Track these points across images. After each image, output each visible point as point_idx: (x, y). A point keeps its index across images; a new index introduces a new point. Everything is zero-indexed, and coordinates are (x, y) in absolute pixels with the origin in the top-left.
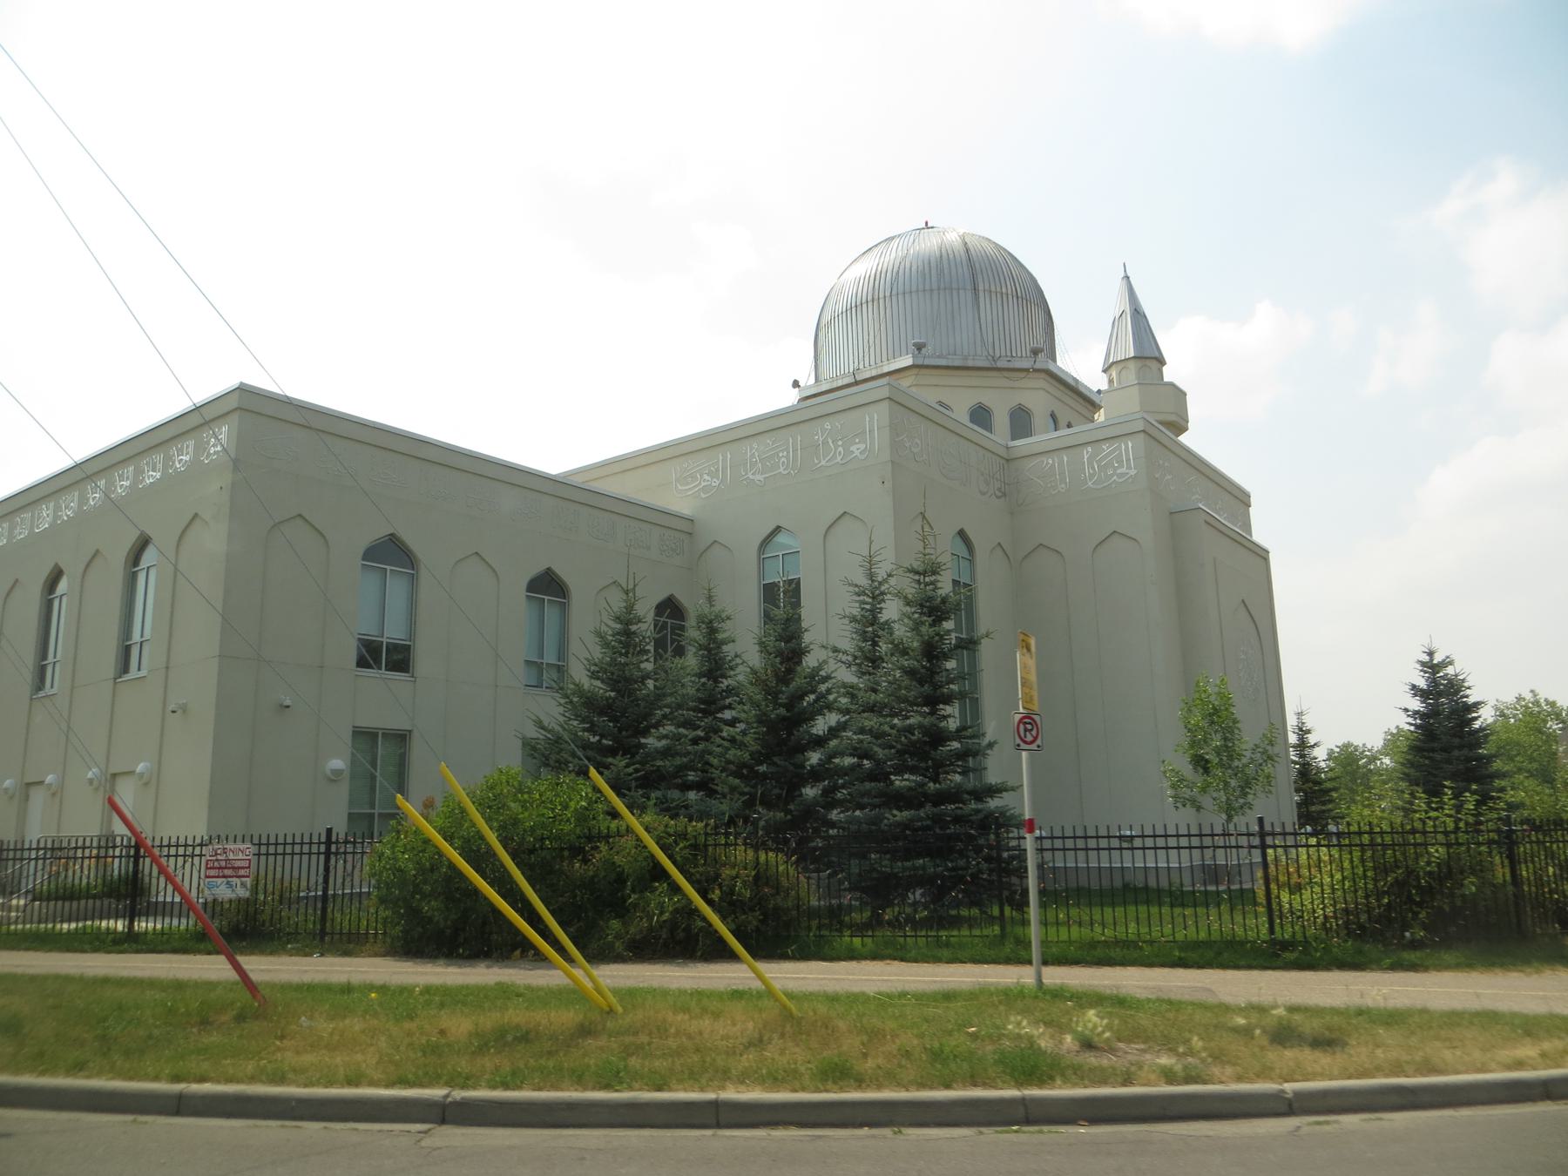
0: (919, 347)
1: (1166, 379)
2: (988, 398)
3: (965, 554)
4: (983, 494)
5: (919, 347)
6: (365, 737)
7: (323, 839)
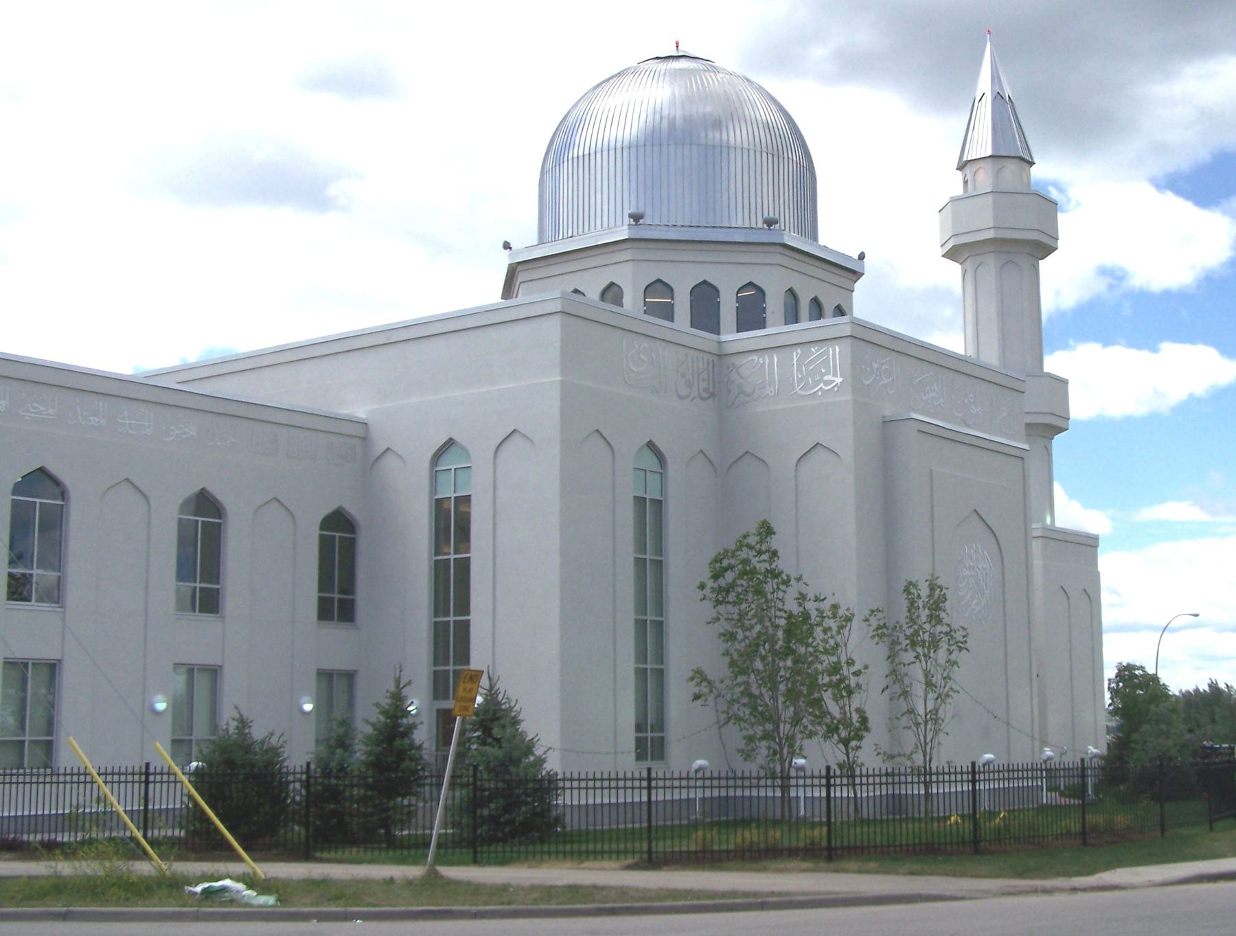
0: (636, 218)
1: (1046, 370)
2: (669, 275)
3: (657, 468)
4: (681, 398)
5: (636, 218)
6: (326, 676)
7: (144, 770)
